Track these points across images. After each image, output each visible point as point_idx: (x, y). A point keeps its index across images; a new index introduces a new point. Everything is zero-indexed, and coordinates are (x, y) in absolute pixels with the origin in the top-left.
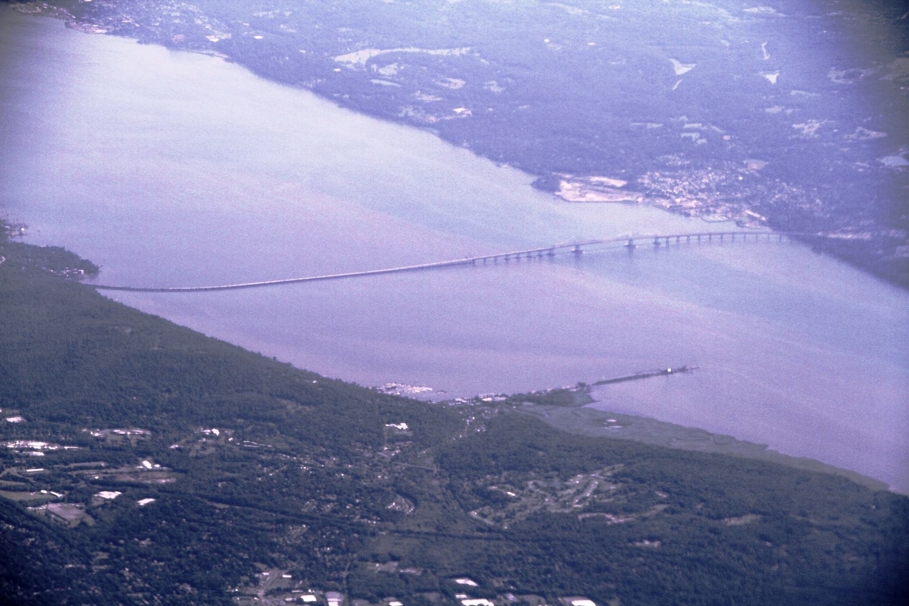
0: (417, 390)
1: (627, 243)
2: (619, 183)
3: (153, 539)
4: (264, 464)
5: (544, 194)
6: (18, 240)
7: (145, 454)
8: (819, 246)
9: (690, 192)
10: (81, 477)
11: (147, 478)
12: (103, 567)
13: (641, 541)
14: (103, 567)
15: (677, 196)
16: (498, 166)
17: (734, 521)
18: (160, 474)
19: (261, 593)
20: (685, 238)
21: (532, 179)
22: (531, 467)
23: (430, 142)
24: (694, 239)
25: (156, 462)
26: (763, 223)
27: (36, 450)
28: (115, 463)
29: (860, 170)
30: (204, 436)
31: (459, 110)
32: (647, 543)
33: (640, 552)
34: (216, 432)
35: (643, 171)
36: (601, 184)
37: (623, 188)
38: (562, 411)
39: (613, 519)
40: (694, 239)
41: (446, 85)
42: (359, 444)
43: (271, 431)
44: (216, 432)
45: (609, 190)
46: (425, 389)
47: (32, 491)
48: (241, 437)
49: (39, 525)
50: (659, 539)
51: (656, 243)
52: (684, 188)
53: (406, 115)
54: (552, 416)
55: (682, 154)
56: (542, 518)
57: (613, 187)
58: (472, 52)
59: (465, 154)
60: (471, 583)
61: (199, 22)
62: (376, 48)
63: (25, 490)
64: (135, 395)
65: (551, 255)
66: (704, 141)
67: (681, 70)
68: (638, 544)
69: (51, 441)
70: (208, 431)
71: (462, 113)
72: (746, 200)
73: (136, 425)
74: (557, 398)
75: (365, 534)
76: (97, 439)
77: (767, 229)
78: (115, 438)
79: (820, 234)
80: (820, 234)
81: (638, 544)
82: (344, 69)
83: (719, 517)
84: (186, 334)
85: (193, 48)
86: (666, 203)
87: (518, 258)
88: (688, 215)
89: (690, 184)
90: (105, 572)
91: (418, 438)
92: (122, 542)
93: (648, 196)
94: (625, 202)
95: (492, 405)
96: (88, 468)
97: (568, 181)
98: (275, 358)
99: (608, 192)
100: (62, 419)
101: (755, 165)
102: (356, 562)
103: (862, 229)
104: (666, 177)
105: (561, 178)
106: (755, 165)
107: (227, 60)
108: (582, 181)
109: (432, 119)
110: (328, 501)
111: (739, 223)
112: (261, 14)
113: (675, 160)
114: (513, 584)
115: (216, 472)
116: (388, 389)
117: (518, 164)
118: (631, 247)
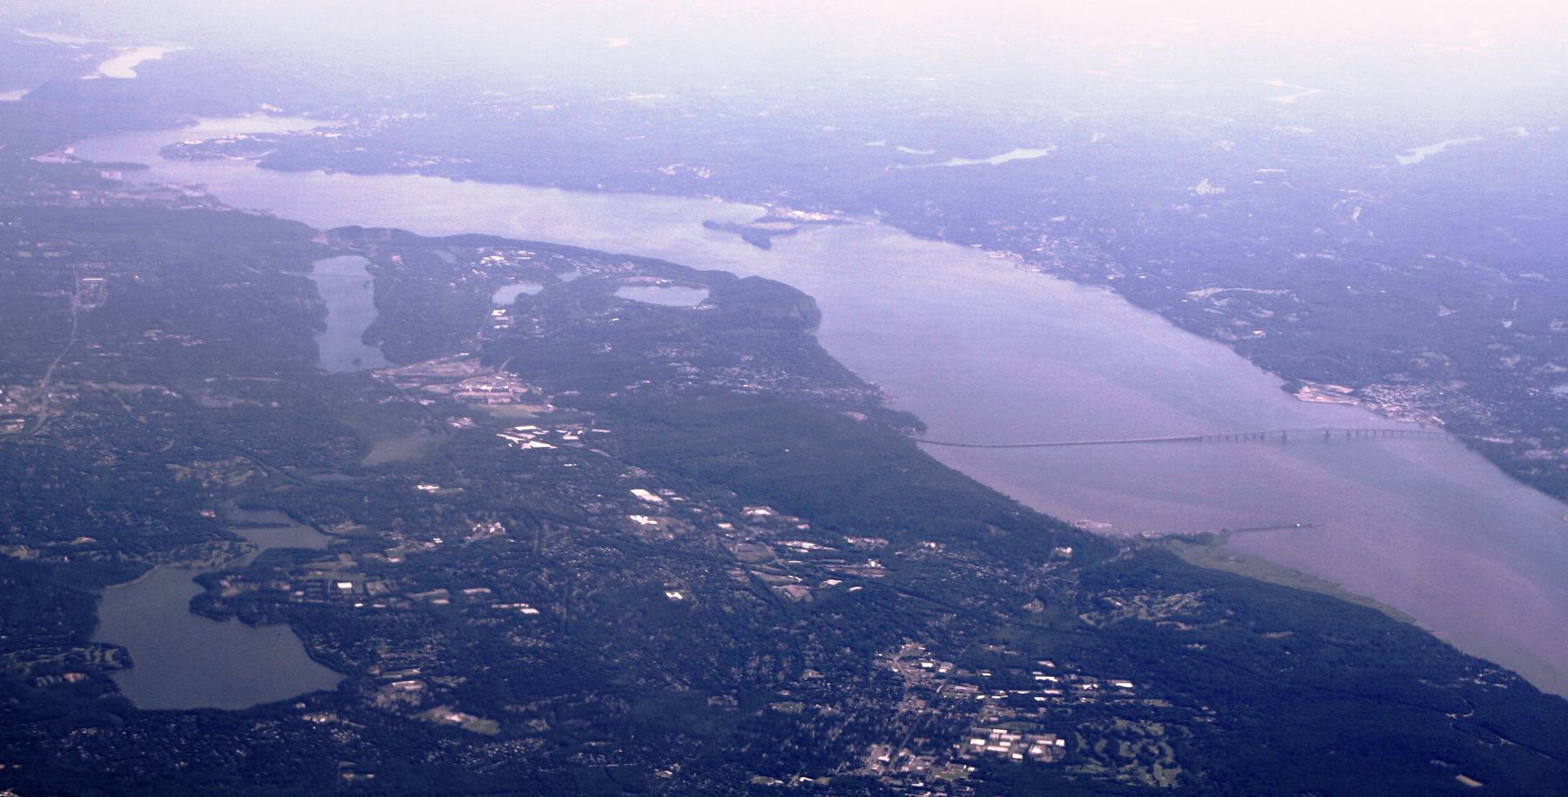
0: (1100, 526)
1: (1324, 433)
2: (1347, 391)
3: (844, 614)
4: (954, 569)
5: (1287, 394)
6: (887, 406)
7: (874, 557)
8: (1472, 445)
9: (1397, 400)
10: (822, 569)
11: (866, 573)
12: (797, 631)
13: (1193, 644)
14: (797, 631)
15: (1385, 403)
16: (1264, 373)
17: (1274, 635)
18: (877, 571)
19: (897, 658)
20: (1363, 432)
21: (1283, 383)
22: (1144, 586)
23: (1227, 354)
24: (1379, 434)
25: (880, 563)
26: (1440, 426)
27: (804, 548)
28: (850, 561)
29: (1531, 394)
30: (923, 547)
31: (1257, 332)
32: (1197, 645)
33: (1186, 651)
34: (933, 545)
35: (1368, 384)
36: (1334, 390)
37: (1349, 394)
38: (1200, 549)
39: (1183, 627)
40: (1379, 434)
41: (1258, 314)
42: (1028, 561)
43: (972, 547)
44: (933, 545)
45: (1338, 395)
46: (1106, 525)
47: (783, 575)
48: (159, 391)
49: (772, 598)
50: (1205, 643)
51: (1348, 434)
52: (1394, 397)
53: (1217, 334)
54: (1189, 555)
55: (1406, 373)
56: (1132, 623)
57: (1342, 393)
58: (1290, 293)
59: (1248, 363)
60: (1050, 665)
61: (1108, 266)
62: (1221, 287)
63: (779, 574)
64: (889, 515)
65: (1262, 438)
66: (1427, 365)
67: (1444, 312)
68: (1189, 646)
69: (817, 543)
70: (927, 545)
71: (1259, 334)
72: (1437, 408)
73: (880, 536)
74: (1202, 540)
75: (995, 624)
76: (850, 544)
77: (1443, 431)
78: (863, 544)
79: (1477, 436)
80: (1477, 436)
81: (1189, 646)
82: (1191, 301)
83: (1264, 631)
84: (973, 483)
85: (1094, 283)
86: (1374, 407)
87: (1236, 438)
88: (1386, 416)
89: (1400, 395)
90: (798, 634)
91: (1075, 560)
92: (822, 615)
93: (1362, 401)
94: (1344, 404)
95: (1149, 540)
96: (830, 563)
97: (1310, 387)
98: (1009, 497)
99: (1333, 396)
100: (833, 529)
101: (1456, 385)
102: (975, 643)
103: (1509, 436)
104: (1385, 388)
105: (1306, 385)
106: (1456, 385)
107: (1113, 292)
108: (1319, 388)
109: (1235, 337)
110: (982, 599)
111: (1422, 425)
112: (1152, 261)
113: (1400, 377)
114: (1079, 667)
115: (918, 573)
116: (1079, 523)
117: (1279, 372)
118: (1327, 436)
